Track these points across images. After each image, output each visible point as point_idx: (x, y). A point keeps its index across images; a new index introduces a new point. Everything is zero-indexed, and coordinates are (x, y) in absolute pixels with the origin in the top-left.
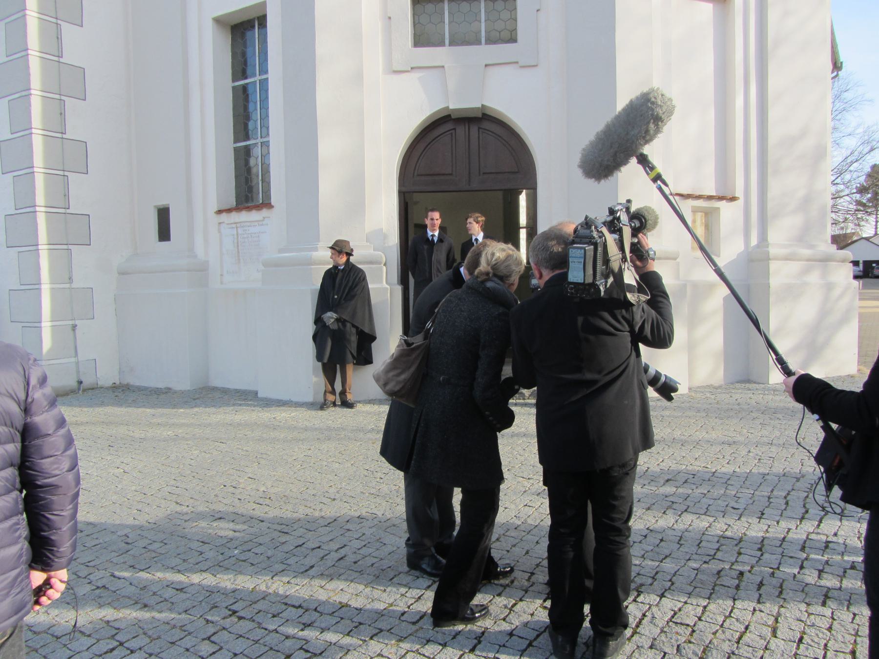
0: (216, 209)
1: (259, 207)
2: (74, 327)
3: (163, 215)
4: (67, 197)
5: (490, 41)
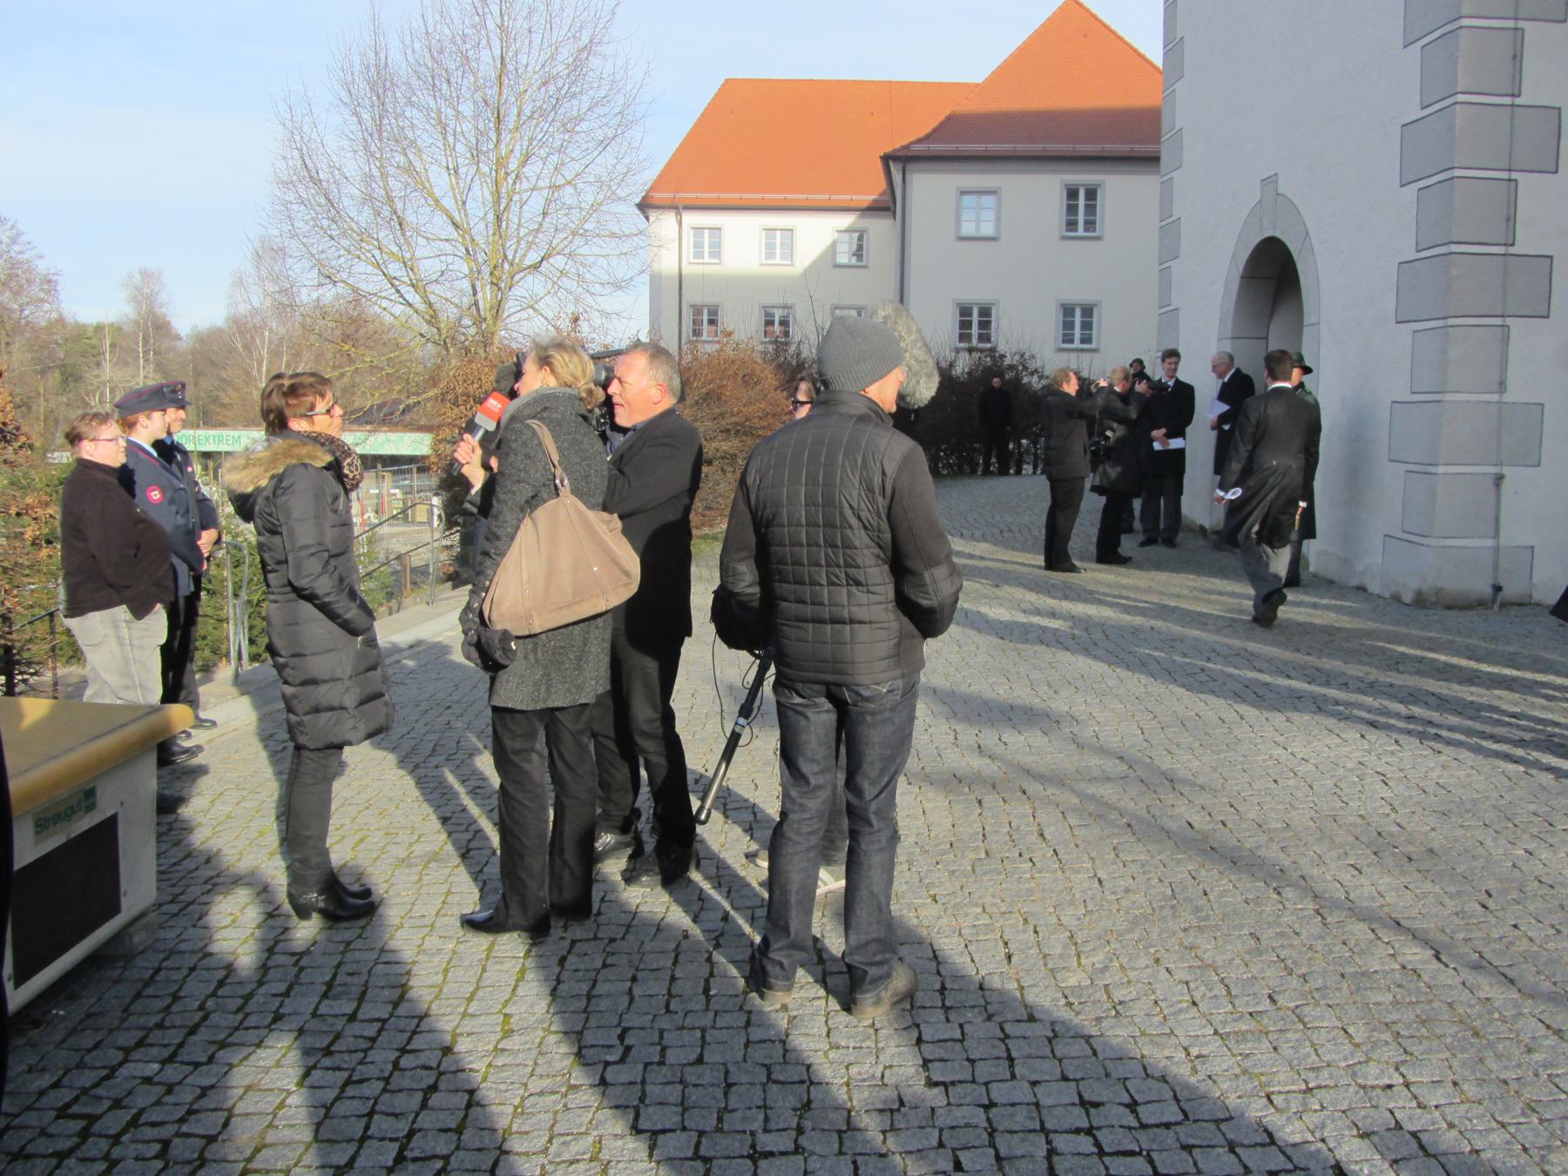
2: (1499, 479)
4: (1511, 222)
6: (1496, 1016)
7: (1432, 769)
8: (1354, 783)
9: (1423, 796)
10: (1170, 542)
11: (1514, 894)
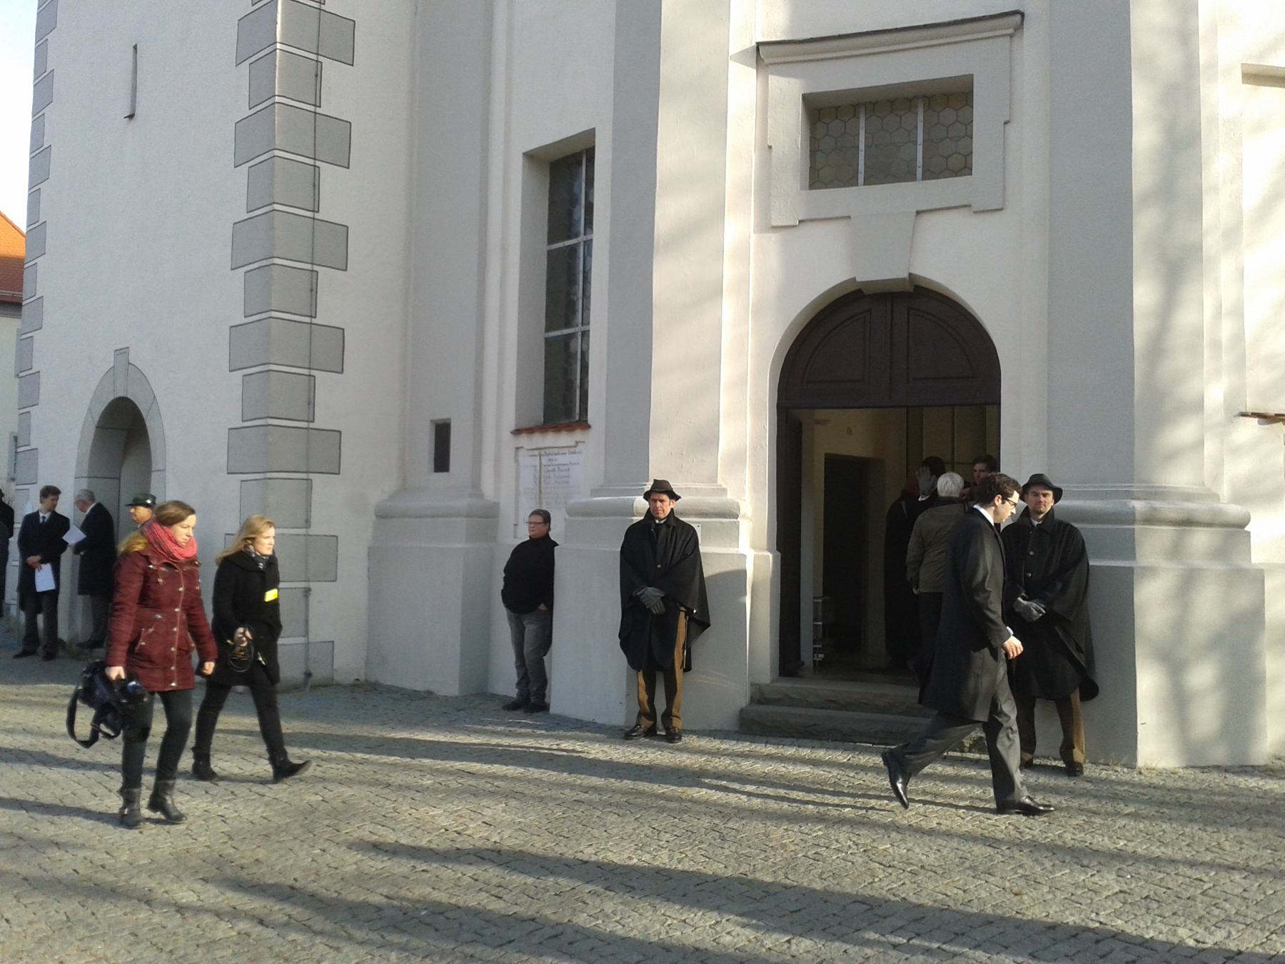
0: (513, 427)
1: (570, 427)
2: (307, 591)
3: (442, 432)
4: (311, 406)
5: (930, 174)
6: (299, 948)
7: (258, 807)
8: (201, 825)
9: (252, 826)
10: (50, 656)
11: (312, 877)
